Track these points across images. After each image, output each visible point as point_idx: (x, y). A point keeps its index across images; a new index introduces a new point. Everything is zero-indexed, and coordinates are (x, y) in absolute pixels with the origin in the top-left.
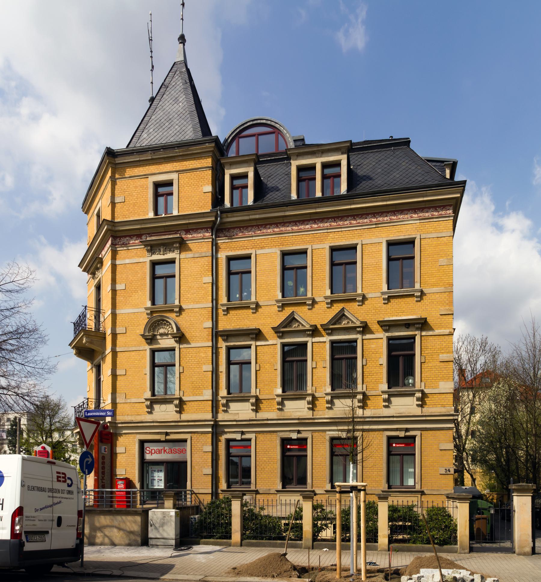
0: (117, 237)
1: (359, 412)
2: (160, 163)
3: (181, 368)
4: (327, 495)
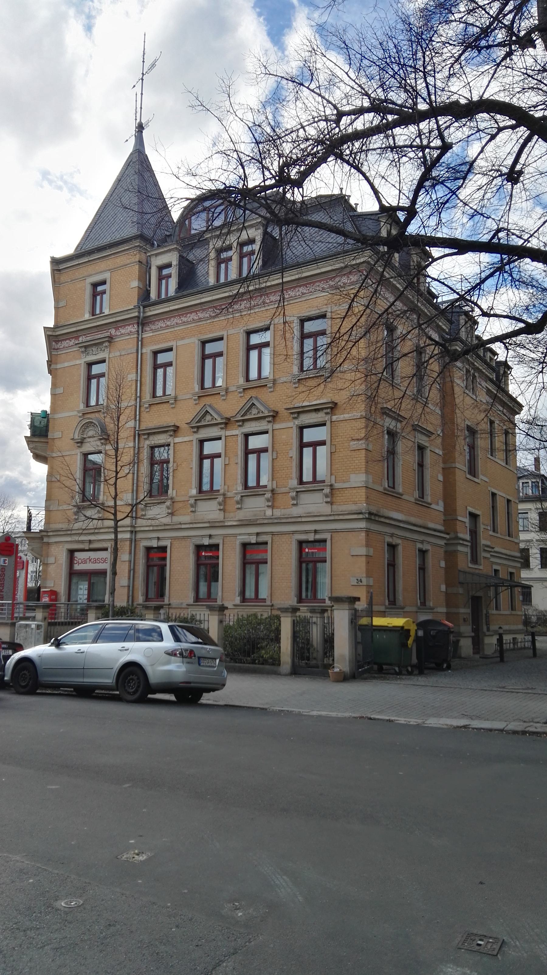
0: (59, 341)
1: (269, 512)
3: (275, 453)
4: (236, 610)
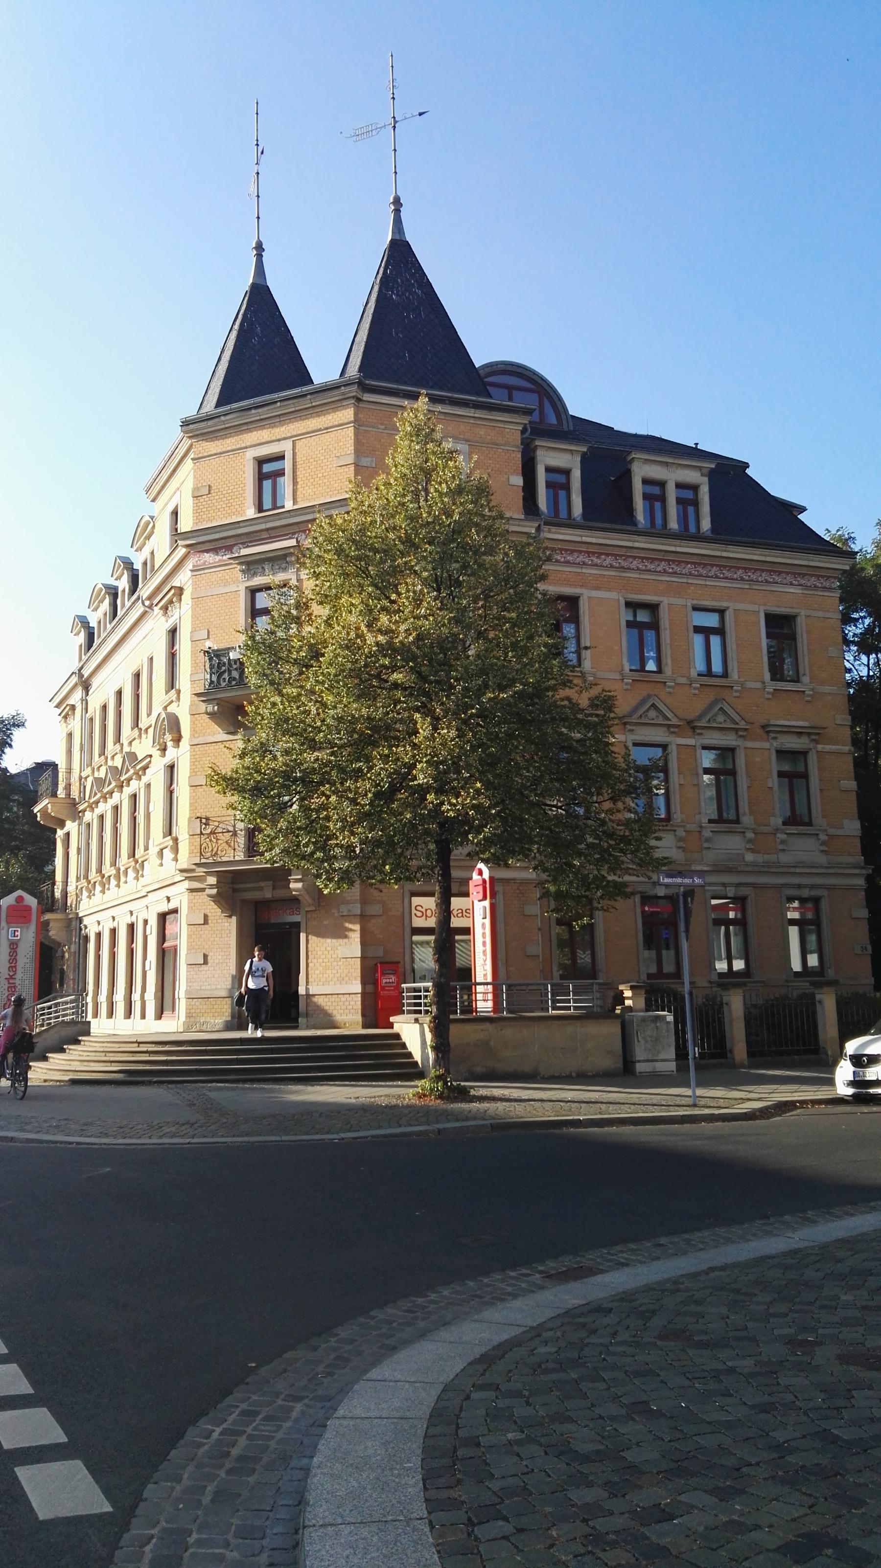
2: (225, 437)
